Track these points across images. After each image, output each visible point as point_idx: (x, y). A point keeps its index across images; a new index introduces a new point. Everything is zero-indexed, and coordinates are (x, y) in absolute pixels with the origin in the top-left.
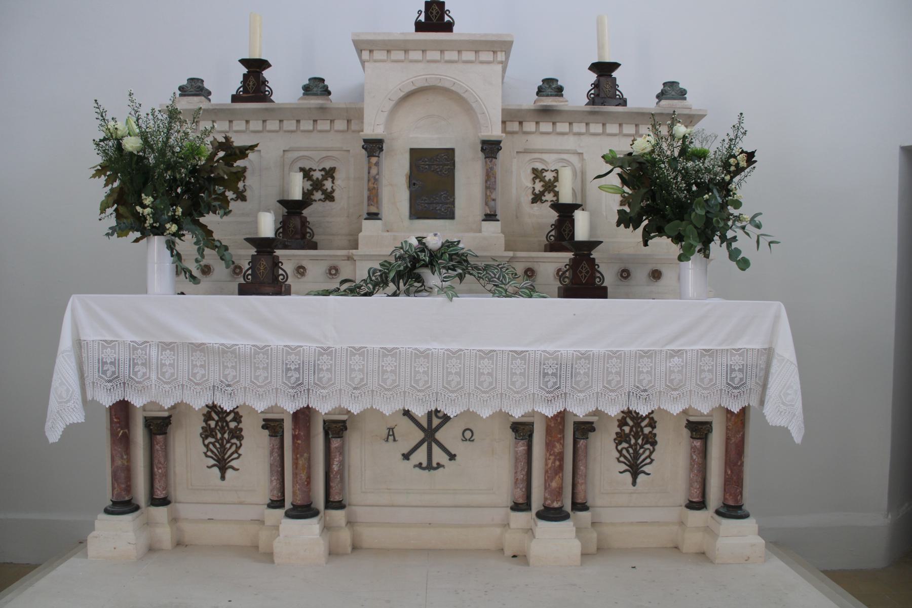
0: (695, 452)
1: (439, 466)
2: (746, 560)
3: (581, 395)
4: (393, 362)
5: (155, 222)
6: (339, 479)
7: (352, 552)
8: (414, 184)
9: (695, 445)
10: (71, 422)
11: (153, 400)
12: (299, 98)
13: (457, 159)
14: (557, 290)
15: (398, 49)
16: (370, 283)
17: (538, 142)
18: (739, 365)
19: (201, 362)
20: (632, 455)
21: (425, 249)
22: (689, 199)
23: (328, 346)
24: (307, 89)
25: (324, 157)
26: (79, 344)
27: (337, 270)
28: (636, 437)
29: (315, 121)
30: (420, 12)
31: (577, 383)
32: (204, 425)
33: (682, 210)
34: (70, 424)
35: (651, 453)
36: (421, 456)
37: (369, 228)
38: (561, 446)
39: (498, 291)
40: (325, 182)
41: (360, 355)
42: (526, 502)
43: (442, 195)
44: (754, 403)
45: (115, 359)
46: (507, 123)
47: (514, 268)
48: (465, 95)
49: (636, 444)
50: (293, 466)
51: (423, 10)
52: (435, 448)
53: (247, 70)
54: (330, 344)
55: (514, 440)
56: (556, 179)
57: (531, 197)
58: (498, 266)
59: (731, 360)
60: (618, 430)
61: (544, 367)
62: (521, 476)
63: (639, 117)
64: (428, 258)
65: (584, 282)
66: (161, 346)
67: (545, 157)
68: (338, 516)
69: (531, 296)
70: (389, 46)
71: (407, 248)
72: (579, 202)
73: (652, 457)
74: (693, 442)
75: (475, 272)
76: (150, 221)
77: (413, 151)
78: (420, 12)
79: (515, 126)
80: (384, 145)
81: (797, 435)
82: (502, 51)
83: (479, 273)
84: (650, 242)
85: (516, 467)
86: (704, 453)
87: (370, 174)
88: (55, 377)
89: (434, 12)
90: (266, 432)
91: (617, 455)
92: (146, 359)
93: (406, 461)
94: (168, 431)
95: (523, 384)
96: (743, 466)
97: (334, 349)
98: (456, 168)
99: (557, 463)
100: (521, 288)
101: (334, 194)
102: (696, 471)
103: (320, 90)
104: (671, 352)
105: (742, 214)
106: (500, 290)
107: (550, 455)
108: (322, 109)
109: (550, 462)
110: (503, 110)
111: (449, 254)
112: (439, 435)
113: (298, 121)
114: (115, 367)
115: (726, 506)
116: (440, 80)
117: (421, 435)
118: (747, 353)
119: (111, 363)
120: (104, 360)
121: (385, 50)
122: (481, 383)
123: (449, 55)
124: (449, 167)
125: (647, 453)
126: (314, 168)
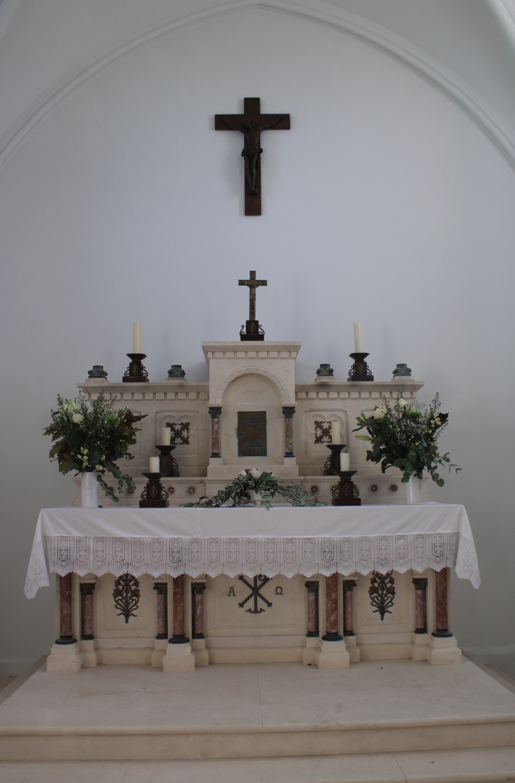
0: (418, 597)
1: (262, 610)
2: (451, 662)
3: (346, 563)
4: (235, 547)
5: (89, 464)
6: (201, 620)
7: (209, 665)
8: (241, 434)
9: (418, 593)
10: (42, 586)
11: (91, 572)
12: (166, 379)
13: (267, 418)
14: (331, 500)
15: (230, 351)
16: (219, 499)
17: (318, 404)
18: (439, 543)
19: (120, 548)
20: (380, 601)
21: (252, 478)
22: (408, 444)
23: (196, 538)
24: (171, 373)
25: (182, 416)
26: (45, 539)
27: (194, 490)
28: (382, 590)
29: (176, 393)
30: (243, 327)
31: (343, 556)
32: (115, 588)
33: (403, 451)
34: (42, 587)
35: (392, 599)
36: (250, 604)
37: (213, 462)
38: (336, 595)
39: (296, 503)
40: (183, 432)
41: (216, 542)
42: (315, 631)
43: (259, 441)
44: (450, 565)
45: (68, 548)
46: (298, 393)
47: (305, 488)
48: (272, 379)
49: (382, 594)
50: (174, 611)
51: (245, 325)
52: (259, 599)
53: (132, 360)
54: (198, 537)
55: (307, 592)
56: (330, 427)
57: (314, 439)
58: (295, 487)
59: (434, 540)
60: (371, 585)
61: (324, 547)
62: (312, 615)
63: (382, 387)
64: (254, 484)
65: (347, 496)
66: (96, 539)
67: (323, 414)
68: (200, 642)
69: (315, 506)
70: (224, 349)
71: (242, 479)
72: (345, 444)
73: (393, 601)
74: (417, 592)
75: (281, 491)
76: (85, 464)
77: (241, 414)
78: (243, 327)
79: (303, 395)
80: (222, 410)
81: (476, 583)
82: (294, 351)
83: (284, 492)
84: (386, 470)
85: (309, 609)
86: (424, 598)
87: (214, 429)
88: (31, 558)
89: (252, 328)
90: (156, 591)
91: (371, 601)
92: (86, 547)
93: (241, 608)
94: (93, 592)
95: (312, 557)
96: (447, 605)
97: (200, 539)
98: (267, 424)
99: (334, 605)
100: (309, 501)
101: (188, 440)
102: (419, 609)
103: (179, 373)
104: (398, 536)
105: (439, 453)
106: (297, 503)
107: (329, 600)
108: (181, 386)
109: (329, 605)
110: (296, 385)
111: (266, 481)
112: (262, 591)
113: (165, 393)
114: (68, 552)
115: (438, 630)
116: (257, 369)
117: (249, 591)
118: (444, 536)
119: (65, 550)
120: (61, 548)
121: (222, 352)
122: (287, 558)
123: (262, 355)
124: (263, 423)
125: (389, 599)
126: (176, 423)
